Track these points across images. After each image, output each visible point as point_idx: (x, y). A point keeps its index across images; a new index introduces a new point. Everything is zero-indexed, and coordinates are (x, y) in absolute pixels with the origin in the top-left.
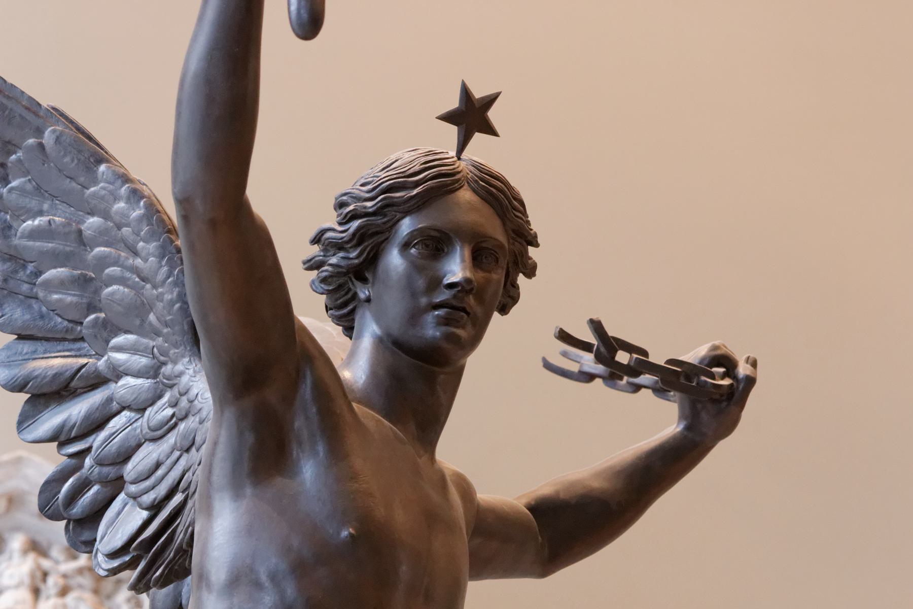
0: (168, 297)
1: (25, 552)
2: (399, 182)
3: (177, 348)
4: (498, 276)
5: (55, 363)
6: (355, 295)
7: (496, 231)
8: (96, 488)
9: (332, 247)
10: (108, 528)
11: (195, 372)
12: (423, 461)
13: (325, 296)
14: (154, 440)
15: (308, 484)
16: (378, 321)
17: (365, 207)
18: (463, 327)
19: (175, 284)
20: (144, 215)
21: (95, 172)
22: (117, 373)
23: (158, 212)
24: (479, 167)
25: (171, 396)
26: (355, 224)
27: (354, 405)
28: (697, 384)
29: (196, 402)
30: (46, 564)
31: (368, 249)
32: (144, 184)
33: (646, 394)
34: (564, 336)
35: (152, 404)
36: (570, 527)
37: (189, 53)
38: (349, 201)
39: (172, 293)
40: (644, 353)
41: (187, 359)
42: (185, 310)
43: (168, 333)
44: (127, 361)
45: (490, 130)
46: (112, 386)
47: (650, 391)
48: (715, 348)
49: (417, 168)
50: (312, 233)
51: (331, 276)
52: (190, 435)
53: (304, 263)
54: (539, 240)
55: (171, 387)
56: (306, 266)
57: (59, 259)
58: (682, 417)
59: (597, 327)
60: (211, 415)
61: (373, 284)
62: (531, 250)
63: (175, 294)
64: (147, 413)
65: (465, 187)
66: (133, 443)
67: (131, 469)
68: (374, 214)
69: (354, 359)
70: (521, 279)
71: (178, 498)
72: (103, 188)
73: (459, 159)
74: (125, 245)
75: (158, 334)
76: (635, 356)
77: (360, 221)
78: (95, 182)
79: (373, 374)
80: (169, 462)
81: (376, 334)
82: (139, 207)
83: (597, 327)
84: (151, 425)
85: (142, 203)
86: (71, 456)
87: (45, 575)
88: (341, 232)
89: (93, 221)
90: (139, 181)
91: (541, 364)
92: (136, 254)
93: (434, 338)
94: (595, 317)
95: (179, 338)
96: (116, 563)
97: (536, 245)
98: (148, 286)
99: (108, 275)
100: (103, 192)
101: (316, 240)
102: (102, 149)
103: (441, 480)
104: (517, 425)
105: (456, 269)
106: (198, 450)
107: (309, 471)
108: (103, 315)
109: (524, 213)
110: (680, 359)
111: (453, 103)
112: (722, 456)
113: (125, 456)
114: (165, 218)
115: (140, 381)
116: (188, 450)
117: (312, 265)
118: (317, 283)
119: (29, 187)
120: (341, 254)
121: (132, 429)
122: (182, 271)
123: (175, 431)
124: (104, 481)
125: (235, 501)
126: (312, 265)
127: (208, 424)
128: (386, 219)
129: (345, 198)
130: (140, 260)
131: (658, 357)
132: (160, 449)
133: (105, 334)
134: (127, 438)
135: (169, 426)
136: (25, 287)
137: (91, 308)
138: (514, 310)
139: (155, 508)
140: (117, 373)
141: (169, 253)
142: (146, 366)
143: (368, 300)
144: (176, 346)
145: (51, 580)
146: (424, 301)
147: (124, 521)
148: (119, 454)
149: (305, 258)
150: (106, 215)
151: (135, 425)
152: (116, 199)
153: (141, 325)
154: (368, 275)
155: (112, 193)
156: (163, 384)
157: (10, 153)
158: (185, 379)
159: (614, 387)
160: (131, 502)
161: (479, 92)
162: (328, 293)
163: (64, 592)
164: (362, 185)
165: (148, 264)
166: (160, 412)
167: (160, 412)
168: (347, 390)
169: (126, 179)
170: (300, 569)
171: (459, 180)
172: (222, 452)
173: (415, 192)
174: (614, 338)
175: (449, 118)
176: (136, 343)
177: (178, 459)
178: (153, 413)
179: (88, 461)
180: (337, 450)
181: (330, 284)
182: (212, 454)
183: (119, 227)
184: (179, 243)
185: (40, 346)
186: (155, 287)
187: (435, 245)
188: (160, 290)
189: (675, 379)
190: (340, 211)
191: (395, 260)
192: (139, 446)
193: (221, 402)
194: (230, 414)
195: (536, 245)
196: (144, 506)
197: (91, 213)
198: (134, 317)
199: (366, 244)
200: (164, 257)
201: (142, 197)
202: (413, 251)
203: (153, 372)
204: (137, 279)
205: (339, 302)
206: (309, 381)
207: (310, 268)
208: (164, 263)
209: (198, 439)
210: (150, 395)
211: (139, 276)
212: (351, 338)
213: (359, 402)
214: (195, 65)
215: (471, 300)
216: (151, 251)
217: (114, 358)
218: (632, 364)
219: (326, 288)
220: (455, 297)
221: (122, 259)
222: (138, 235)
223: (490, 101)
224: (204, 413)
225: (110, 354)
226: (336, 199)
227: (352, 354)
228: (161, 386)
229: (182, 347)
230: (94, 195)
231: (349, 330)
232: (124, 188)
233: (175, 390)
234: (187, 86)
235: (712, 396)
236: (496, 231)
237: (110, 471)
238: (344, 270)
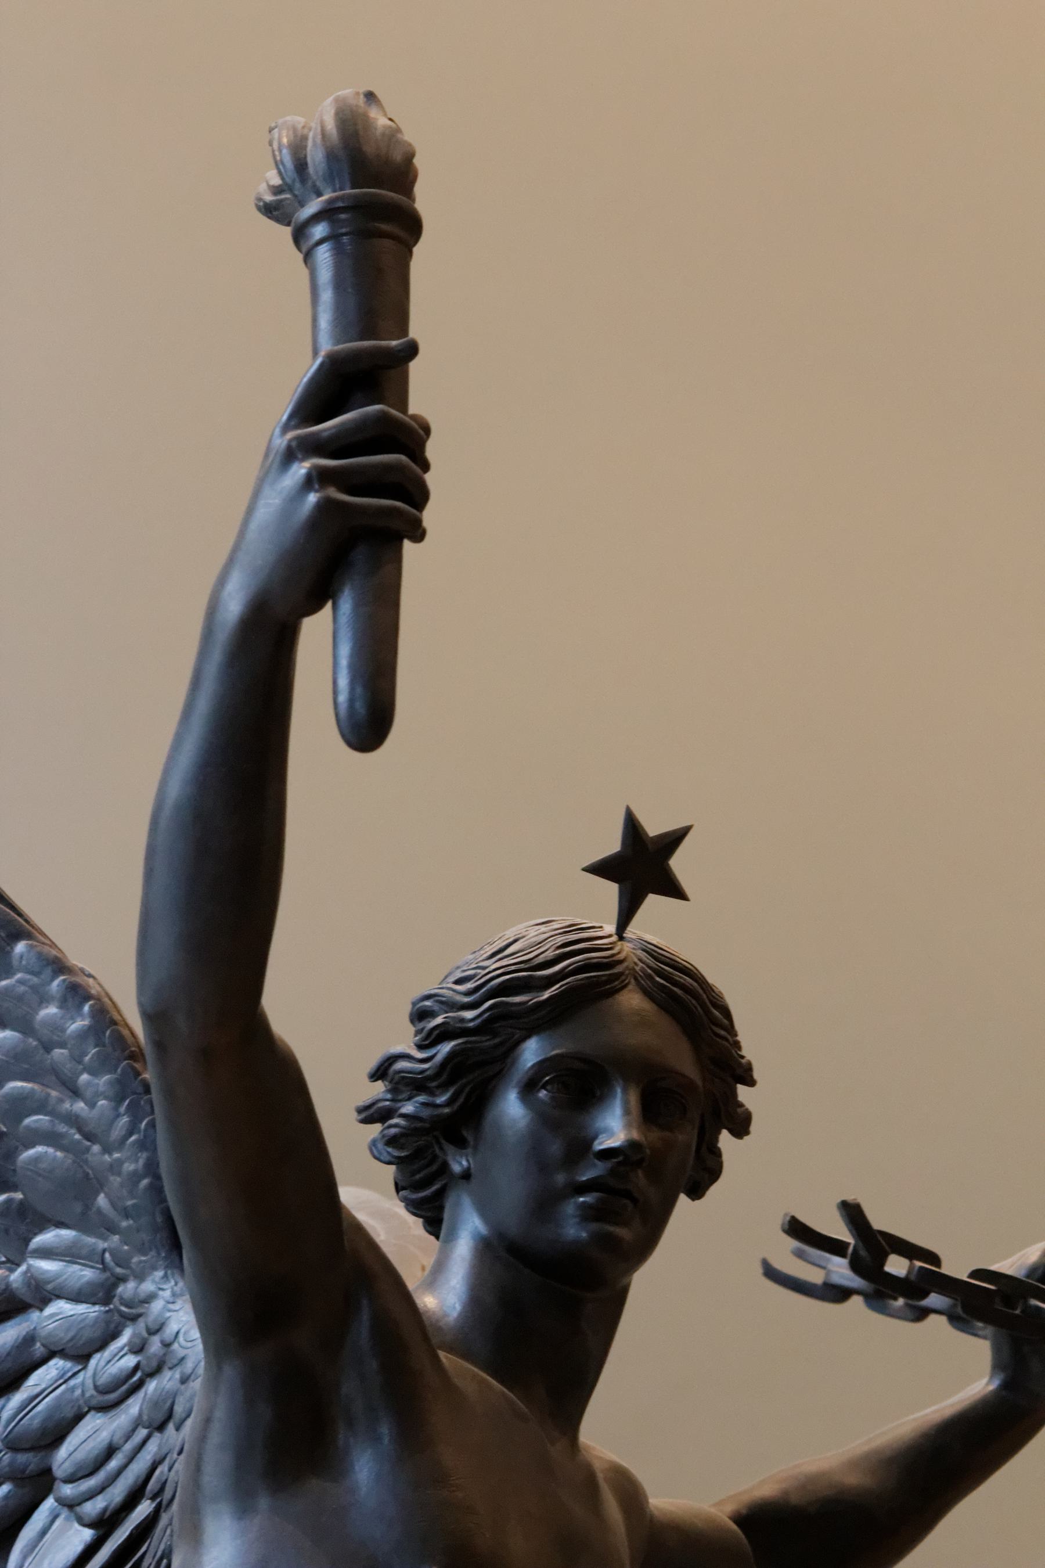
0: (129, 1167)
2: (518, 978)
3: (145, 1255)
4: (686, 1136)
6: (445, 1167)
7: (682, 1059)
9: (407, 1085)
10: (25, 1558)
11: (174, 1295)
13: (393, 1168)
14: (105, 1408)
15: (364, 1490)
16: (483, 1211)
17: (462, 1020)
18: (625, 1224)
19: (142, 1145)
20: (90, 1028)
21: (8, 954)
22: (42, 1294)
23: (114, 1023)
24: (654, 953)
25: (134, 1335)
26: (445, 1048)
27: (442, 1354)
28: (1023, 1311)
29: (175, 1346)
31: (467, 1090)
32: (90, 976)
33: (937, 1323)
34: (797, 1229)
35: (102, 1346)
37: (171, 759)
38: (436, 1008)
39: (137, 1161)
40: (933, 1258)
41: (160, 1273)
42: (157, 1189)
43: (129, 1227)
44: (58, 1275)
45: (673, 890)
46: (35, 1315)
47: (943, 1320)
49: (550, 954)
50: (372, 1062)
51: (402, 1135)
52: (164, 1401)
53: (360, 1110)
54: (756, 1075)
55: (134, 1319)
56: (363, 1116)
58: (998, 1366)
59: (853, 1213)
60: (201, 1370)
61: (476, 1148)
62: (743, 1093)
63: (141, 1162)
64: (93, 1362)
65: (630, 987)
66: (69, 1413)
67: (66, 1456)
69: (440, 1275)
70: (725, 1140)
71: (144, 1509)
72: (20, 982)
73: (621, 938)
74: (57, 1076)
75: (112, 1229)
76: (918, 1264)
77: (453, 1043)
79: (475, 1300)
80: (128, 1447)
81: (479, 1233)
82: (81, 1015)
83: (853, 1213)
84: (99, 1383)
85: (86, 1008)
90: (82, 970)
91: (760, 1270)
92: (75, 1093)
94: (850, 1198)
95: (145, 1236)
97: (751, 1082)
98: (96, 1148)
99: (28, 1127)
100: (22, 989)
101: (380, 1073)
102: (20, 914)
103: (587, 1481)
104: (722, 1378)
105: (614, 1127)
106: (178, 1428)
108: (19, 1196)
109: (731, 1029)
110: (994, 1267)
111: (610, 843)
113: (56, 1432)
114: (125, 1032)
115: (81, 1308)
116: (161, 1427)
117: (371, 1114)
118: (380, 1146)
120: (422, 1098)
121: (67, 1390)
122: (152, 1125)
123: (141, 1394)
125: (240, 1519)
126: (371, 1114)
127: (196, 1385)
128: (497, 1040)
129: (428, 1003)
130: (82, 1104)
132: (115, 1424)
133: (23, 1228)
134: (57, 1406)
135: (128, 1386)
138: (714, 1191)
140: (42, 1294)
141: (130, 1091)
142: (89, 1283)
143: (466, 1175)
144: (142, 1250)
146: (560, 1178)
148: (43, 1431)
149: (361, 1102)
150: (25, 1026)
151: (72, 1383)
152: (44, 1000)
153: (84, 1214)
154: (468, 1135)
155: (34, 989)
156: (122, 1315)
158: (157, 1306)
159: (883, 1310)
160: (65, 1513)
161: (654, 827)
162: (398, 1162)
164: (458, 982)
165: (95, 1112)
166: (115, 1361)
167: (115, 1361)
168: (427, 1323)
169: (59, 966)
171: (621, 974)
172: (216, 1436)
173: (546, 995)
174: (881, 1233)
175: (602, 869)
176: (75, 1243)
177: (144, 1442)
178: (102, 1363)
180: (412, 1435)
181: (401, 1148)
182: (202, 1438)
183: (48, 1048)
184: (146, 1076)
186: (107, 1150)
187: (576, 1086)
188: (116, 1155)
190: (421, 1025)
191: (512, 1109)
192: (79, 1418)
193: (218, 1349)
194: (230, 1371)
195: (751, 1082)
196: (87, 1520)
198: (72, 1198)
199: (464, 1081)
200: (123, 1099)
201: (88, 997)
202: (543, 1094)
203: (102, 1293)
204: (77, 1136)
205: (418, 1177)
206: (365, 1316)
207: (367, 1121)
208: (122, 1109)
209: (179, 1410)
210: (98, 1333)
211: (80, 1130)
212: (437, 1238)
213: (450, 1349)
214: (175, 790)
215: (640, 1179)
216: (101, 1089)
217: (39, 1268)
218: (913, 1277)
219: (396, 1153)
220: (612, 1172)
221: (52, 1101)
222: (80, 1062)
223: (674, 840)
224: (189, 1365)
225: (32, 1261)
226: (414, 1004)
227: (439, 1268)
228: (116, 1317)
229: (153, 1253)
231: (434, 1225)
232: (56, 983)
233: (141, 1324)
234: (163, 823)
236: (682, 1059)
237: (27, 1460)
238: (427, 1125)
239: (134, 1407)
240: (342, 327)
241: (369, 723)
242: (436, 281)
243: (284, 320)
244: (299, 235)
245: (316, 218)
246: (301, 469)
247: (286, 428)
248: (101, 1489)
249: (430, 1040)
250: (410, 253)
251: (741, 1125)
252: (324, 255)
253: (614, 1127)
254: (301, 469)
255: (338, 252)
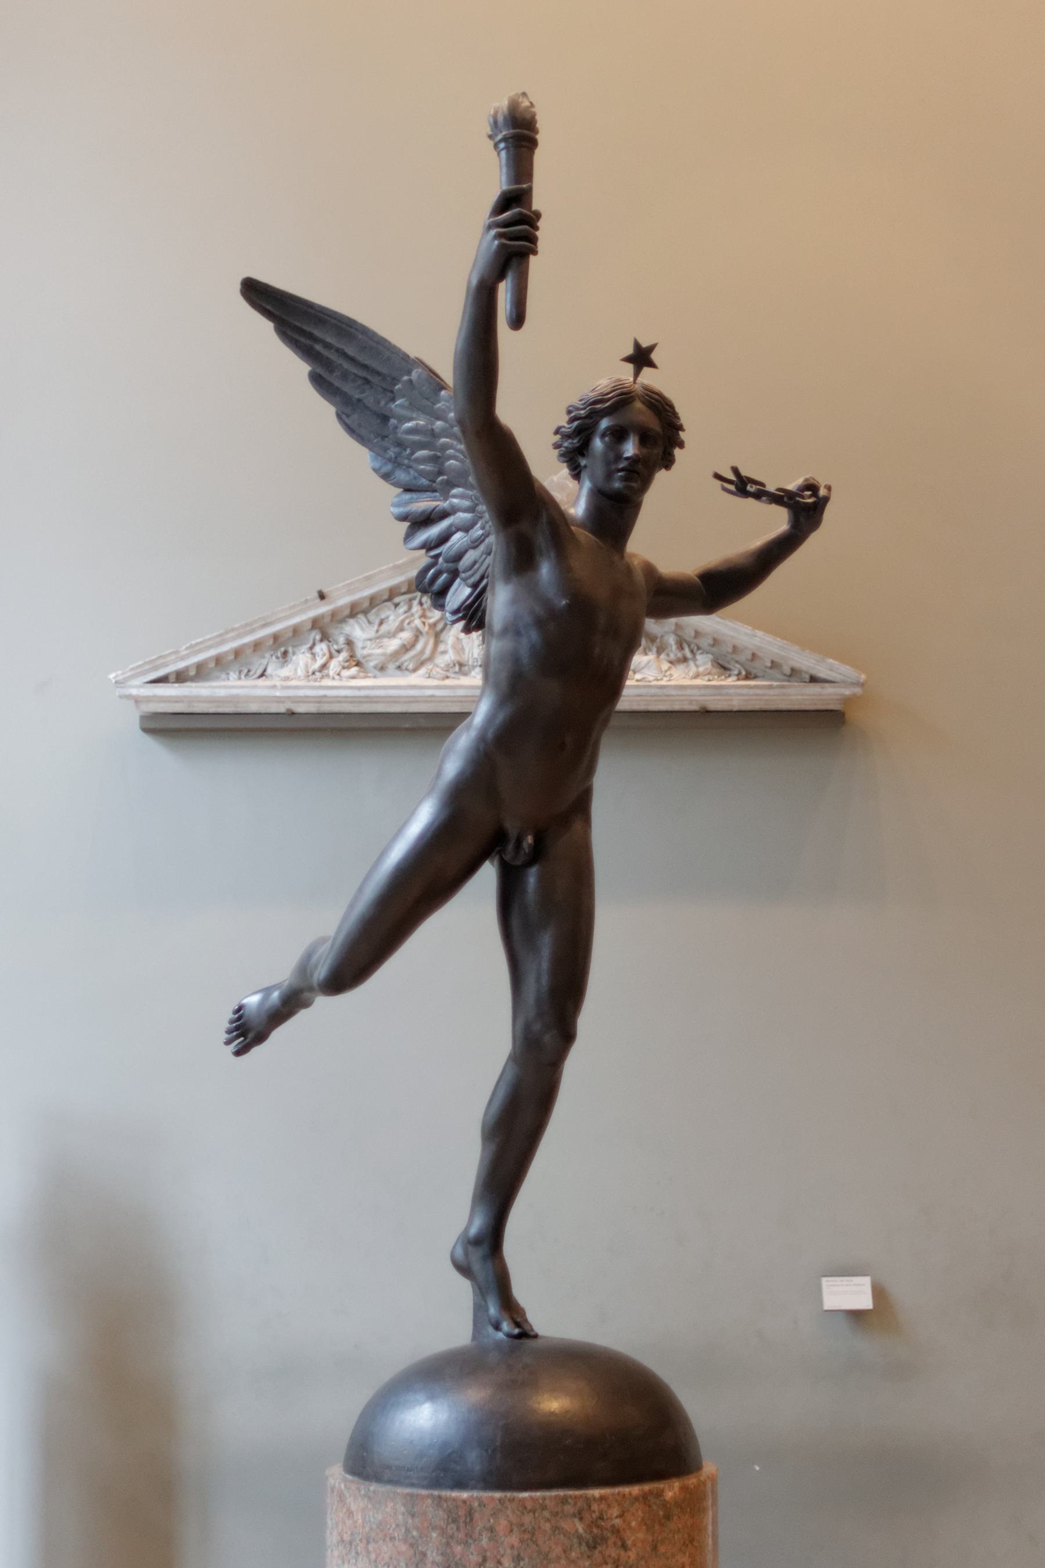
4: (658, 451)
5: (423, 504)
7: (653, 423)
8: (445, 576)
12: (616, 558)
14: (475, 548)
16: (591, 481)
18: (636, 481)
24: (646, 388)
26: (576, 423)
34: (718, 476)
36: (723, 586)
40: (762, 485)
57: (423, 446)
59: (735, 471)
68: (586, 417)
71: (485, 582)
78: (439, 402)
79: (588, 509)
83: (735, 471)
86: (432, 557)
88: (568, 428)
89: (439, 423)
93: (619, 488)
96: (455, 618)
97: (683, 430)
101: (557, 432)
105: (630, 449)
107: (546, 570)
111: (629, 351)
113: (459, 557)
124: (448, 571)
131: (771, 488)
136: (406, 462)
137: (440, 473)
139: (474, 586)
143: (585, 466)
147: (460, 593)
157: (395, 385)
161: (645, 344)
170: (540, 623)
173: (607, 404)
179: (441, 560)
185: (414, 495)
187: (618, 435)
189: (781, 498)
192: (466, 551)
195: (683, 430)
197: (438, 419)
213: (577, 526)
214: (459, 346)
230: (439, 409)
235: (806, 509)
236: (653, 423)
239: (482, 547)
240: (510, 182)
242: (542, 159)
243: (493, 178)
244: (496, 146)
245: (500, 141)
246: (493, 232)
247: (490, 217)
248: (473, 575)
249: (571, 421)
250: (533, 153)
251: (681, 445)
252: (503, 154)
253: (630, 449)
254: (493, 232)
255: (508, 153)
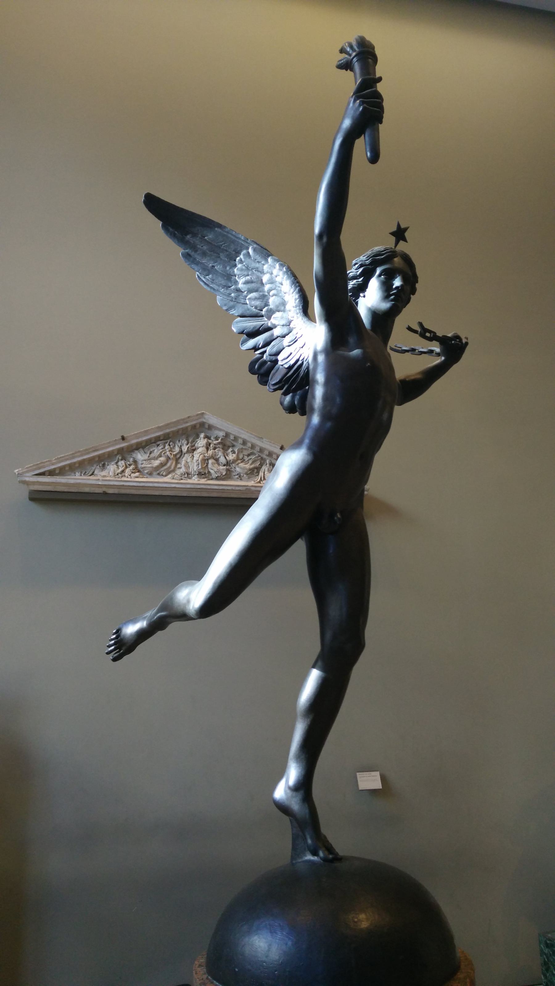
1: (204, 438)
7: (407, 269)
30: (210, 441)
40: (435, 333)
48: (455, 333)
59: (421, 324)
67: (280, 357)
68: (369, 265)
83: (421, 324)
87: (210, 444)
95: (298, 311)
105: (397, 282)
111: (394, 229)
112: (455, 368)
119: (244, 268)
145: (211, 446)
163: (215, 449)
173: (382, 257)
189: (444, 341)
235: (453, 349)
236: (407, 269)
237: (273, 358)
241: (375, 158)
